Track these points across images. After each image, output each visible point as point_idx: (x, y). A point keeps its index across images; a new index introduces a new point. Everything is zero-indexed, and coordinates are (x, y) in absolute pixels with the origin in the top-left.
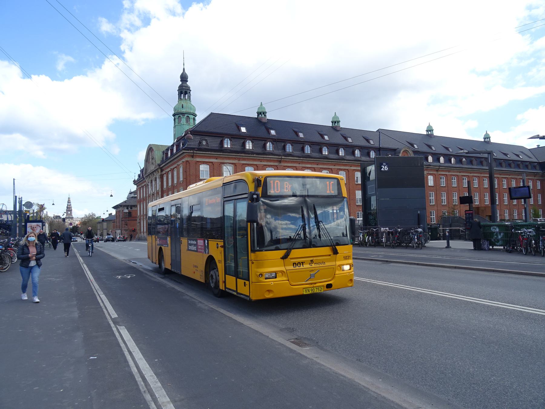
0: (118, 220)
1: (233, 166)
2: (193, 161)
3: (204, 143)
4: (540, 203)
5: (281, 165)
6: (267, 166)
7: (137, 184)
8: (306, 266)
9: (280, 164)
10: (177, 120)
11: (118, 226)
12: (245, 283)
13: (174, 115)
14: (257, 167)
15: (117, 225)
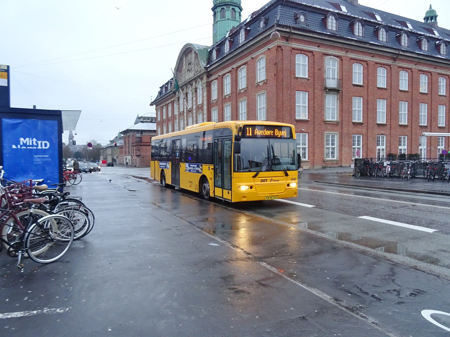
1: (338, 60)
2: (287, 47)
3: (302, 18)
4: (249, 134)
7: (156, 103)
8: (268, 182)
9: (394, 64)
10: (219, 15)
12: (228, 192)
13: (213, 9)
14: (368, 64)
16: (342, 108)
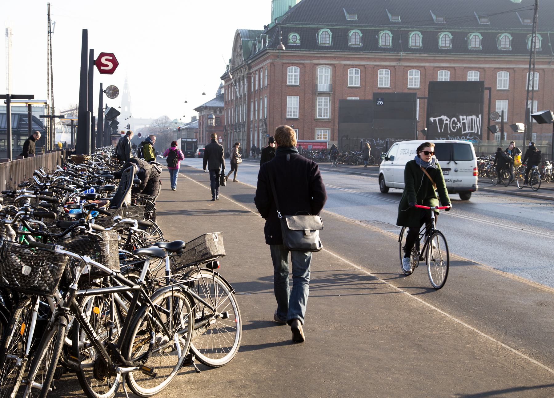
0: (201, 129)
5: (400, 64)
6: (410, 68)
11: (201, 138)
14: (365, 68)
15: (200, 137)
16: (334, 108)
